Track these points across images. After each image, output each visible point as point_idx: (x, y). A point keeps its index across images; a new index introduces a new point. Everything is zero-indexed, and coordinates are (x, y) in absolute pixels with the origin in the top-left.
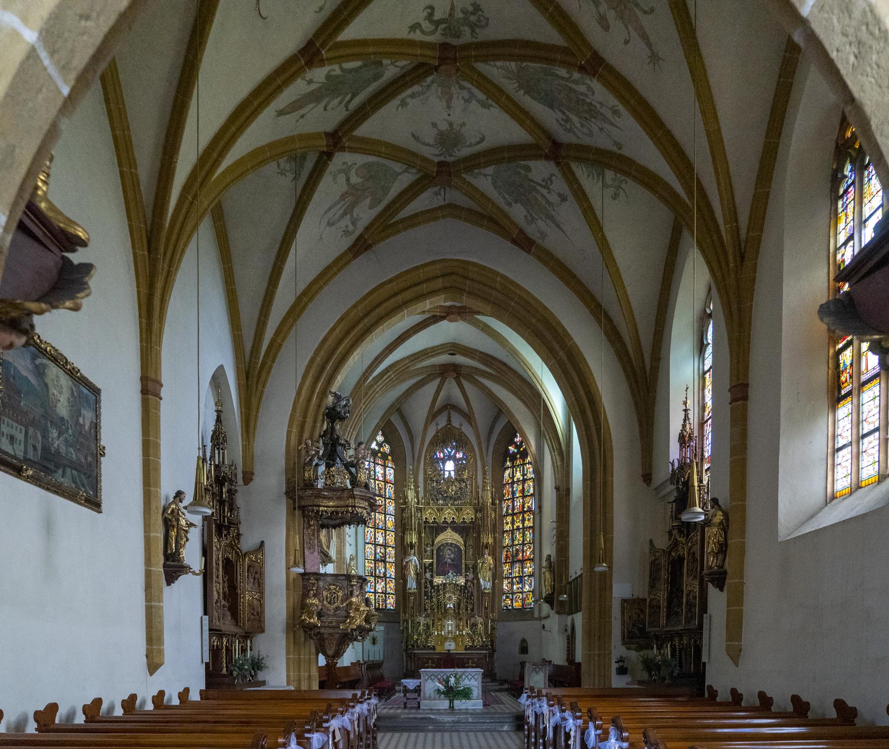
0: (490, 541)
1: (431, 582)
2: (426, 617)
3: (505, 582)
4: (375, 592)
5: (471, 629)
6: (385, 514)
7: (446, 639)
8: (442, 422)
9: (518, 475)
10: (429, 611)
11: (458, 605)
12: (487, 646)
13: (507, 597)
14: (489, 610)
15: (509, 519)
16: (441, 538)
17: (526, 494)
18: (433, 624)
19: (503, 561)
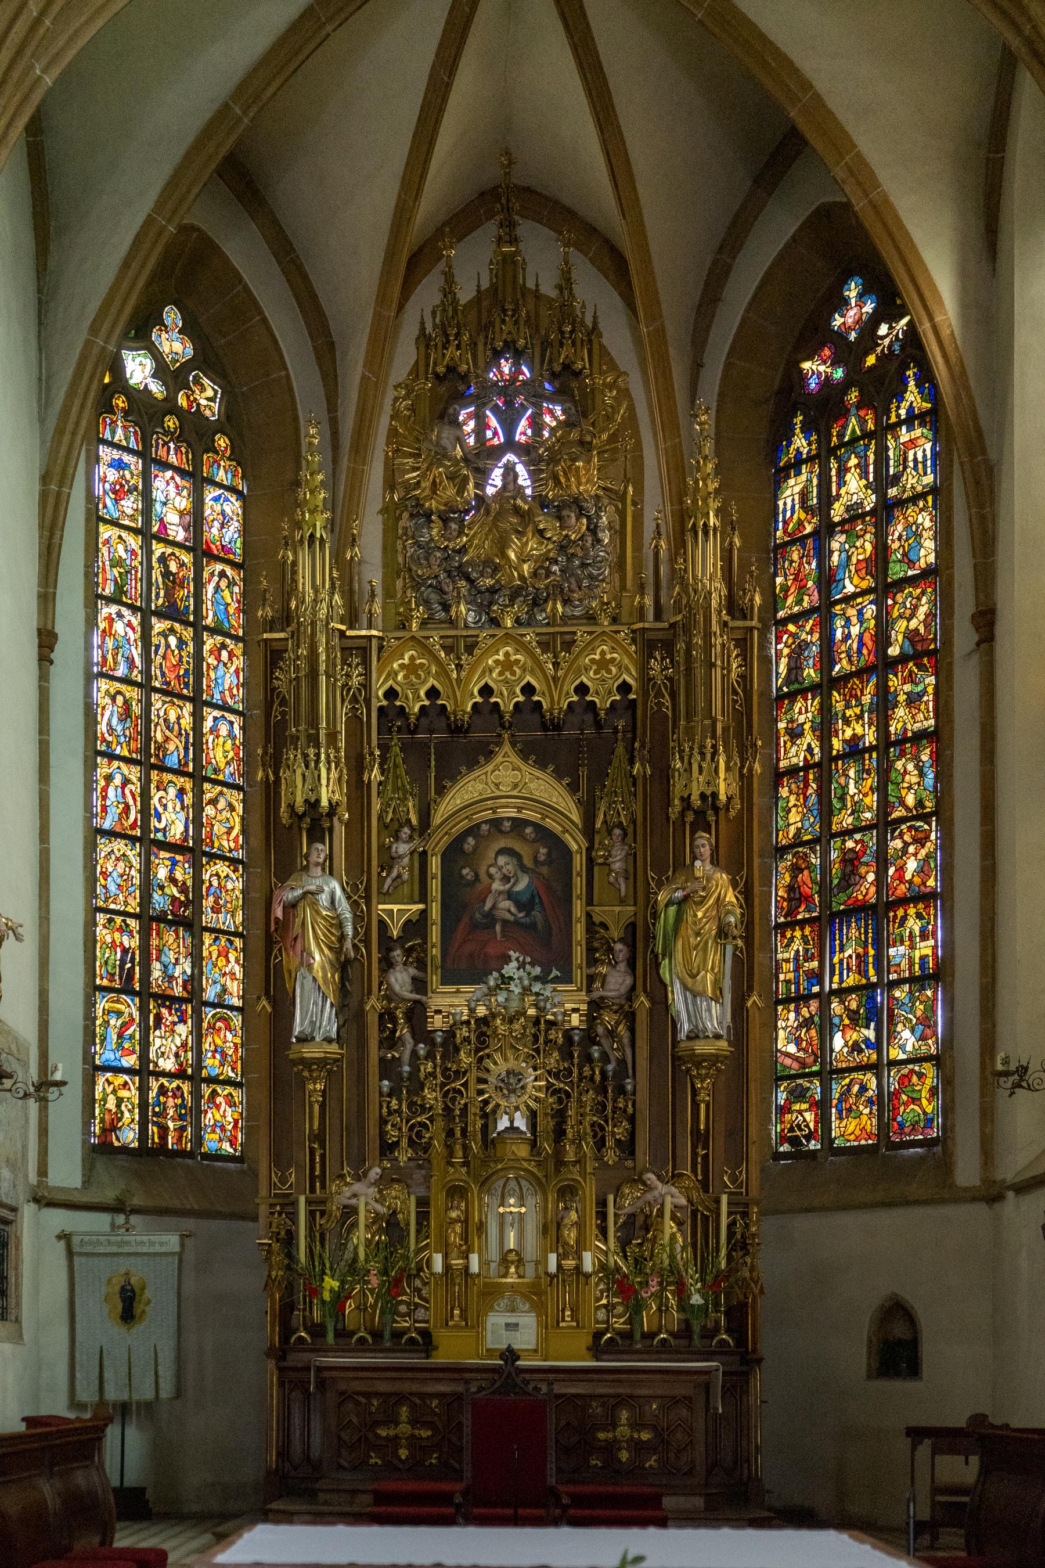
0: (724, 787)
1: (417, 1014)
2: (385, 1181)
3: (788, 1018)
4: (144, 1071)
5: (624, 1244)
6: (199, 703)
7: (491, 1293)
8: (471, 266)
9: (854, 488)
10: (404, 1156)
11: (553, 1125)
12: (709, 1334)
13: (799, 1094)
14: (717, 1146)
15: (805, 712)
16: (468, 791)
17: (897, 571)
18: (423, 1217)
19: (776, 917)
